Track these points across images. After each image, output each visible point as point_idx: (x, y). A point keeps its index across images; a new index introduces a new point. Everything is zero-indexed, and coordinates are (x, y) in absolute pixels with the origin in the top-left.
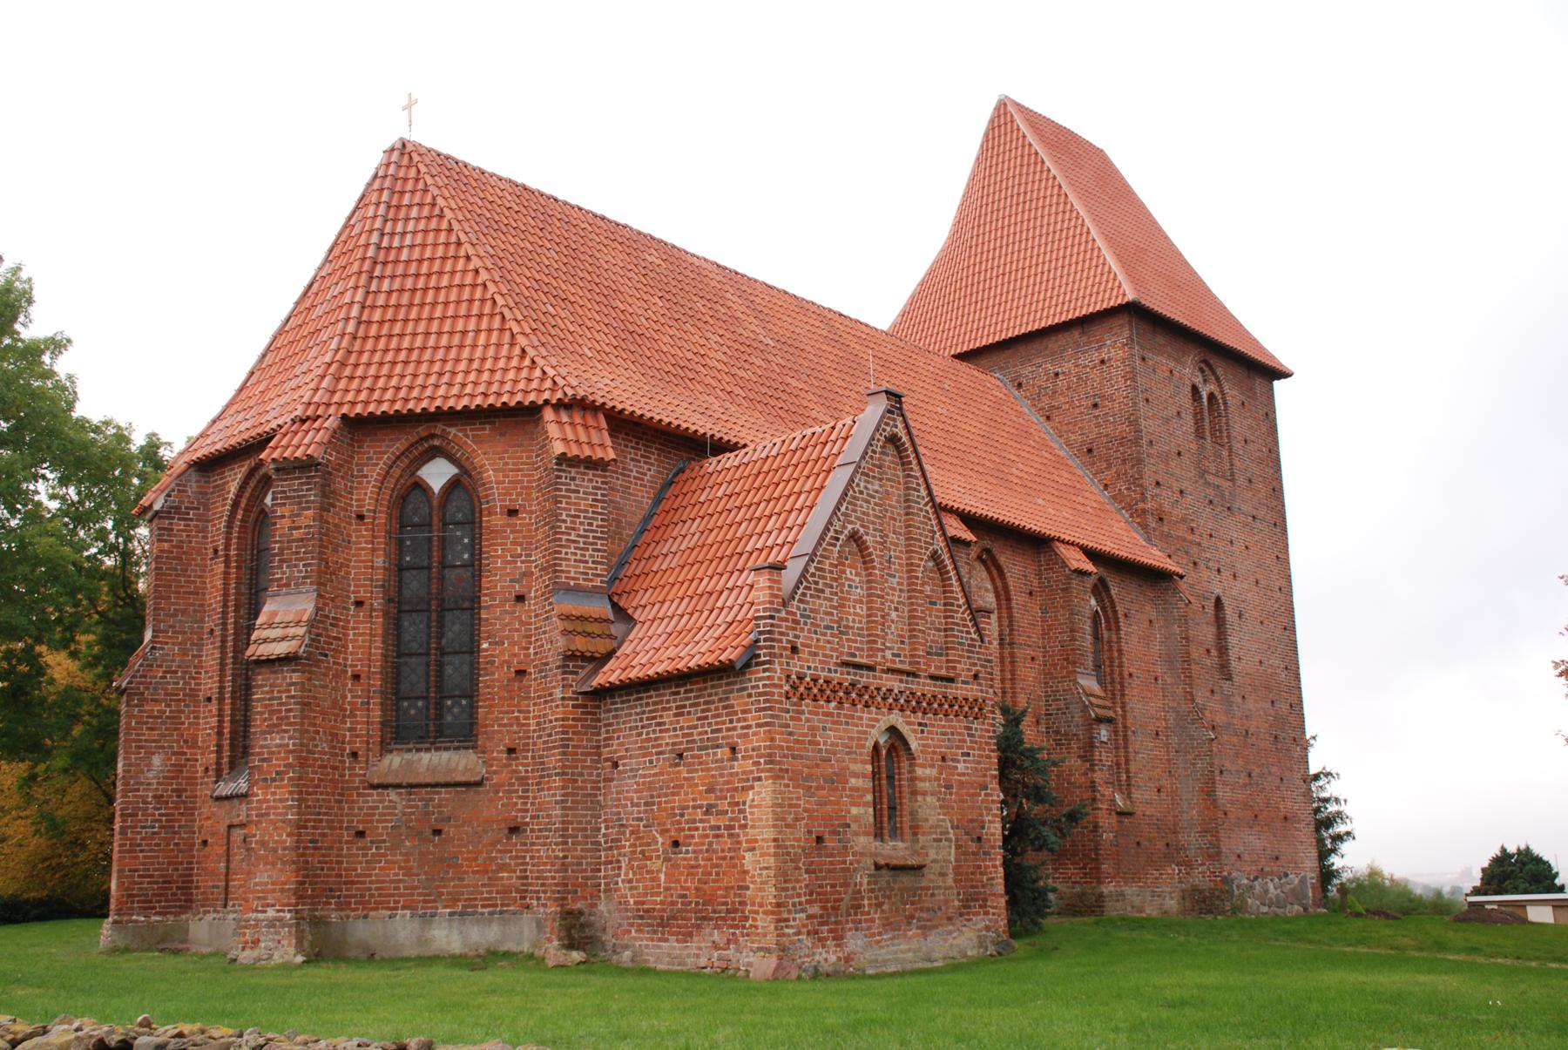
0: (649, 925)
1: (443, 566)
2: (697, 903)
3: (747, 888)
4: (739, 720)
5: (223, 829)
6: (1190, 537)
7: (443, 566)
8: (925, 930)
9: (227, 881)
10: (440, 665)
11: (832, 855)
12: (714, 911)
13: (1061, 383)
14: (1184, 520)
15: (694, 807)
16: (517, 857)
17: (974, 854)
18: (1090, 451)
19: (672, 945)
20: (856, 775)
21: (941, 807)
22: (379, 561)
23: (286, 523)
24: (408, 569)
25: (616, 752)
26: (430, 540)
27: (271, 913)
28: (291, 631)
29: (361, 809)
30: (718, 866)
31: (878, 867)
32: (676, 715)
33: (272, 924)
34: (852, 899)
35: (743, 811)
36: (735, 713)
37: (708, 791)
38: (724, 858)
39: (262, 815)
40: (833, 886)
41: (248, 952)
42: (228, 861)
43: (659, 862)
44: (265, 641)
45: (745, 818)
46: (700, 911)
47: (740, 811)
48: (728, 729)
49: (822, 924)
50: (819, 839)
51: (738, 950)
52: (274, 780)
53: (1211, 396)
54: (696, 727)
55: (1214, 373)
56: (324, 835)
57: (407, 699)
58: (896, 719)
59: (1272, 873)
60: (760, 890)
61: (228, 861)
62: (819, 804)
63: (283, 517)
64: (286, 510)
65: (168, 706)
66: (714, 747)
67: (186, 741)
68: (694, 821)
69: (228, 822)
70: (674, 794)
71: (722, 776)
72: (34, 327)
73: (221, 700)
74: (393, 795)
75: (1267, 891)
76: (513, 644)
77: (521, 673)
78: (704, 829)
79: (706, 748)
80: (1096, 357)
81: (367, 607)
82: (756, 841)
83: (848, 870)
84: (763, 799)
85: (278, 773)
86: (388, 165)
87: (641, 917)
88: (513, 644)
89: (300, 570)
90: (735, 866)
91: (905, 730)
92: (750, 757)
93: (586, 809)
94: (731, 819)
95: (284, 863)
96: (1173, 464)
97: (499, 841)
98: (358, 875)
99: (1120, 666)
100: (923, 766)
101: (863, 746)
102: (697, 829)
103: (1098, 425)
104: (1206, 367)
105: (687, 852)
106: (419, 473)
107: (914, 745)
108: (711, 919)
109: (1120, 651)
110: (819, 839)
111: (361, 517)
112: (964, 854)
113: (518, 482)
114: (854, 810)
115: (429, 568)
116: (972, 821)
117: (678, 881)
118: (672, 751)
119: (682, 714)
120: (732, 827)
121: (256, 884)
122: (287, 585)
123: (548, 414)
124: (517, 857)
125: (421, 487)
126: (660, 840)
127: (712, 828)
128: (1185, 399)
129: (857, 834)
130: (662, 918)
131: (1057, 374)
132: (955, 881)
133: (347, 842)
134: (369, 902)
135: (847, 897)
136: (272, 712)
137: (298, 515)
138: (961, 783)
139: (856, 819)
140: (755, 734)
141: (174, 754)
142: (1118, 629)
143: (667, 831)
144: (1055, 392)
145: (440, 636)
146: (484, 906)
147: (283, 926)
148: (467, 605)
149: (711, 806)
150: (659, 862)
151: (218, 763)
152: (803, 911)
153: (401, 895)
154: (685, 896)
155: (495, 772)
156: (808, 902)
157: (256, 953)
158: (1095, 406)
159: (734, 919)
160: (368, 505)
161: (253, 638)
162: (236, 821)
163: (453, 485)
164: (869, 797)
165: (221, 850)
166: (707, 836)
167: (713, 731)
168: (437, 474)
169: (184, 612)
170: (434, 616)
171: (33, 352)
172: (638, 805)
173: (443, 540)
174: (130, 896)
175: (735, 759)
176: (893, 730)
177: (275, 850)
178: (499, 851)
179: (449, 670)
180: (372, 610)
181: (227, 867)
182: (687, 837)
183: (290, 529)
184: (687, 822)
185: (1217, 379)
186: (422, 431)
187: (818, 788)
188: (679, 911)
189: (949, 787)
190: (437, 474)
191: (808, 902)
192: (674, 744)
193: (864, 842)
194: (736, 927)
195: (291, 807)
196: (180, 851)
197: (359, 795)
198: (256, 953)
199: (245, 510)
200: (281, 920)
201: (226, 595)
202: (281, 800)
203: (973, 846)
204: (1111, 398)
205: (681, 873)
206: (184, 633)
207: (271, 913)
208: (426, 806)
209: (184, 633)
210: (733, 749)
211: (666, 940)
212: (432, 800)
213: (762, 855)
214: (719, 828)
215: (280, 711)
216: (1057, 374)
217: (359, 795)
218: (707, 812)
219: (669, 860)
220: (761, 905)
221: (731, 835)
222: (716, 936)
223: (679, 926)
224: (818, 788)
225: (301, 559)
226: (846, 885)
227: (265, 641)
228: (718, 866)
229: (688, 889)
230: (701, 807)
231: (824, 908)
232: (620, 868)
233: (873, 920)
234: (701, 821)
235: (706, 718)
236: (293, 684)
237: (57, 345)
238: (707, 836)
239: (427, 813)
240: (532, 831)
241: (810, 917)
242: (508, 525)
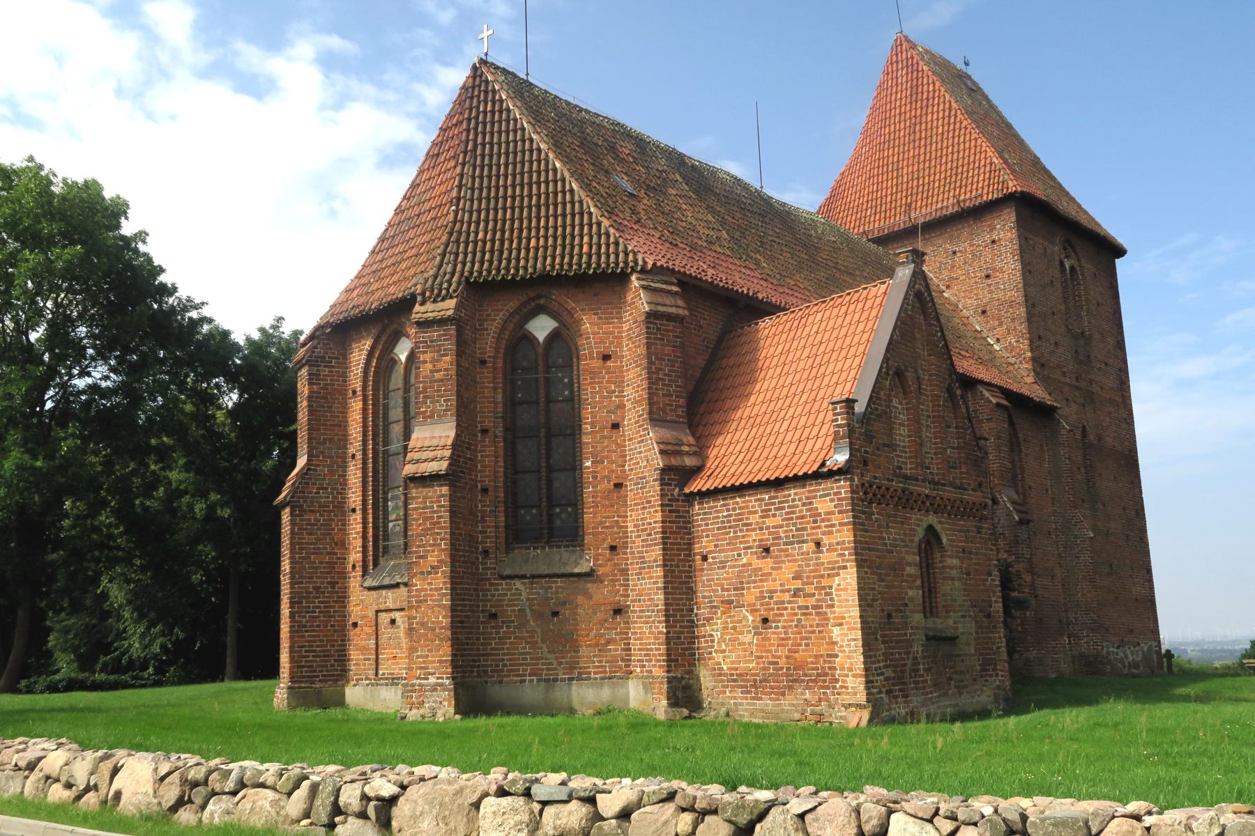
0: (742, 687)
1: (549, 401)
2: (788, 669)
3: (837, 656)
4: (823, 520)
5: (371, 614)
6: (1063, 379)
7: (549, 401)
8: (960, 689)
9: (377, 655)
10: (549, 481)
11: (898, 629)
12: (805, 675)
13: (959, 259)
14: (1059, 366)
15: (782, 591)
16: (621, 633)
17: (987, 628)
18: (984, 312)
19: (767, 703)
20: (909, 564)
21: (965, 590)
22: (500, 398)
23: (429, 366)
24: (521, 403)
25: (706, 547)
26: (537, 380)
27: (432, 680)
28: (439, 453)
29: (493, 595)
30: (806, 638)
31: (928, 638)
32: (761, 517)
33: (434, 688)
34: (913, 664)
35: (831, 594)
36: (819, 515)
37: (794, 578)
38: (813, 632)
39: (421, 601)
40: (900, 654)
41: (414, 711)
42: (377, 639)
43: (750, 636)
44: (418, 461)
45: (832, 599)
46: (791, 675)
47: (827, 594)
48: (813, 528)
49: (894, 685)
50: (889, 616)
51: (831, 706)
52: (429, 573)
53: (1072, 268)
54: (781, 526)
55: (1074, 250)
56: (468, 617)
57: (558, 506)
58: (932, 519)
59: (1128, 643)
60: (849, 657)
61: (377, 639)
62: (887, 587)
63: (425, 362)
64: (428, 357)
65: (322, 515)
66: (798, 542)
67: (336, 544)
68: (783, 602)
69: (376, 608)
70: (762, 581)
71: (808, 565)
72: (128, 228)
73: (364, 510)
74: (518, 584)
75: (1126, 657)
76: (611, 462)
77: (618, 486)
78: (792, 609)
79: (792, 543)
80: (987, 238)
81: (491, 434)
82: (844, 618)
83: (907, 641)
84: (849, 584)
85: (433, 567)
86: (473, 88)
87: (734, 681)
88: (611, 462)
89: (441, 405)
90: (823, 638)
91: (938, 527)
92: (835, 550)
93: (683, 593)
94: (818, 600)
95: (440, 640)
96: (1049, 322)
97: (606, 621)
98: (493, 649)
99: (1023, 480)
100: (951, 557)
101: (913, 541)
102: (786, 609)
103: (991, 292)
104: (1068, 245)
105: (777, 627)
106: (527, 327)
107: (944, 541)
108: (803, 681)
109: (1022, 469)
110: (889, 616)
111: (483, 362)
112: (980, 627)
113: (611, 333)
114: (910, 593)
115: (537, 403)
116: (984, 601)
117: (770, 651)
118: (759, 547)
119: (768, 516)
120: (821, 607)
121: (418, 657)
122: (432, 417)
123: (635, 281)
124: (621, 633)
125: (530, 338)
126: (751, 618)
127: (800, 608)
128: (1056, 273)
129: (912, 612)
130: (755, 681)
131: (955, 253)
132: (976, 649)
133: (483, 623)
134: (502, 671)
135: (909, 663)
136: (425, 519)
137: (439, 361)
138: (976, 570)
139: (912, 600)
140: (838, 531)
141: (328, 553)
142: (1020, 451)
143: (757, 610)
144: (953, 267)
145: (548, 457)
146: (595, 673)
147: (444, 690)
148: (569, 432)
149: (798, 590)
150: (750, 636)
151: (365, 561)
152: (882, 674)
153: (528, 665)
154: (777, 663)
155: (600, 565)
156: (886, 667)
157: (422, 711)
158: (988, 276)
159: (824, 681)
160: (489, 351)
161: (408, 458)
162: (382, 607)
163: (554, 336)
164: (919, 582)
165: (371, 630)
166: (796, 614)
167: (797, 530)
168: (541, 328)
169: (331, 440)
170: (543, 441)
171: (127, 242)
172: (728, 590)
173: (547, 380)
174: (299, 667)
175: (822, 552)
176: (930, 529)
177: (433, 629)
178: (606, 629)
179: (556, 484)
180: (496, 436)
181: (377, 644)
182: (776, 615)
183: (432, 371)
184: (776, 603)
185: (1077, 255)
186: (532, 294)
187: (886, 575)
188: (771, 675)
189: (968, 574)
190: (541, 328)
191: (886, 667)
192: (761, 540)
193: (918, 618)
194: (828, 688)
195: (445, 595)
196: (335, 631)
197: (491, 585)
198: (422, 711)
199: (378, 359)
200: (441, 685)
201: (365, 427)
202: (436, 589)
203: (986, 622)
204: (1001, 271)
205: (773, 645)
206: (331, 457)
207: (432, 680)
208: (546, 592)
209: (331, 457)
210: (818, 544)
211: (761, 699)
212: (551, 588)
213: (849, 629)
214: (807, 607)
215: (432, 518)
216: (955, 253)
217: (491, 585)
218: (795, 595)
219: (761, 633)
220: (850, 669)
221: (817, 614)
222: (808, 695)
223: (771, 687)
224: (886, 575)
225: (442, 396)
226: (908, 653)
227: (418, 461)
228: (806, 638)
229: (780, 657)
230: (788, 591)
231: (895, 672)
232: (713, 641)
233: (926, 681)
234: (789, 602)
235: (791, 519)
236: (442, 496)
237: (142, 236)
238: (796, 614)
239: (547, 599)
240: (635, 612)
241: (887, 679)
242: (604, 368)
